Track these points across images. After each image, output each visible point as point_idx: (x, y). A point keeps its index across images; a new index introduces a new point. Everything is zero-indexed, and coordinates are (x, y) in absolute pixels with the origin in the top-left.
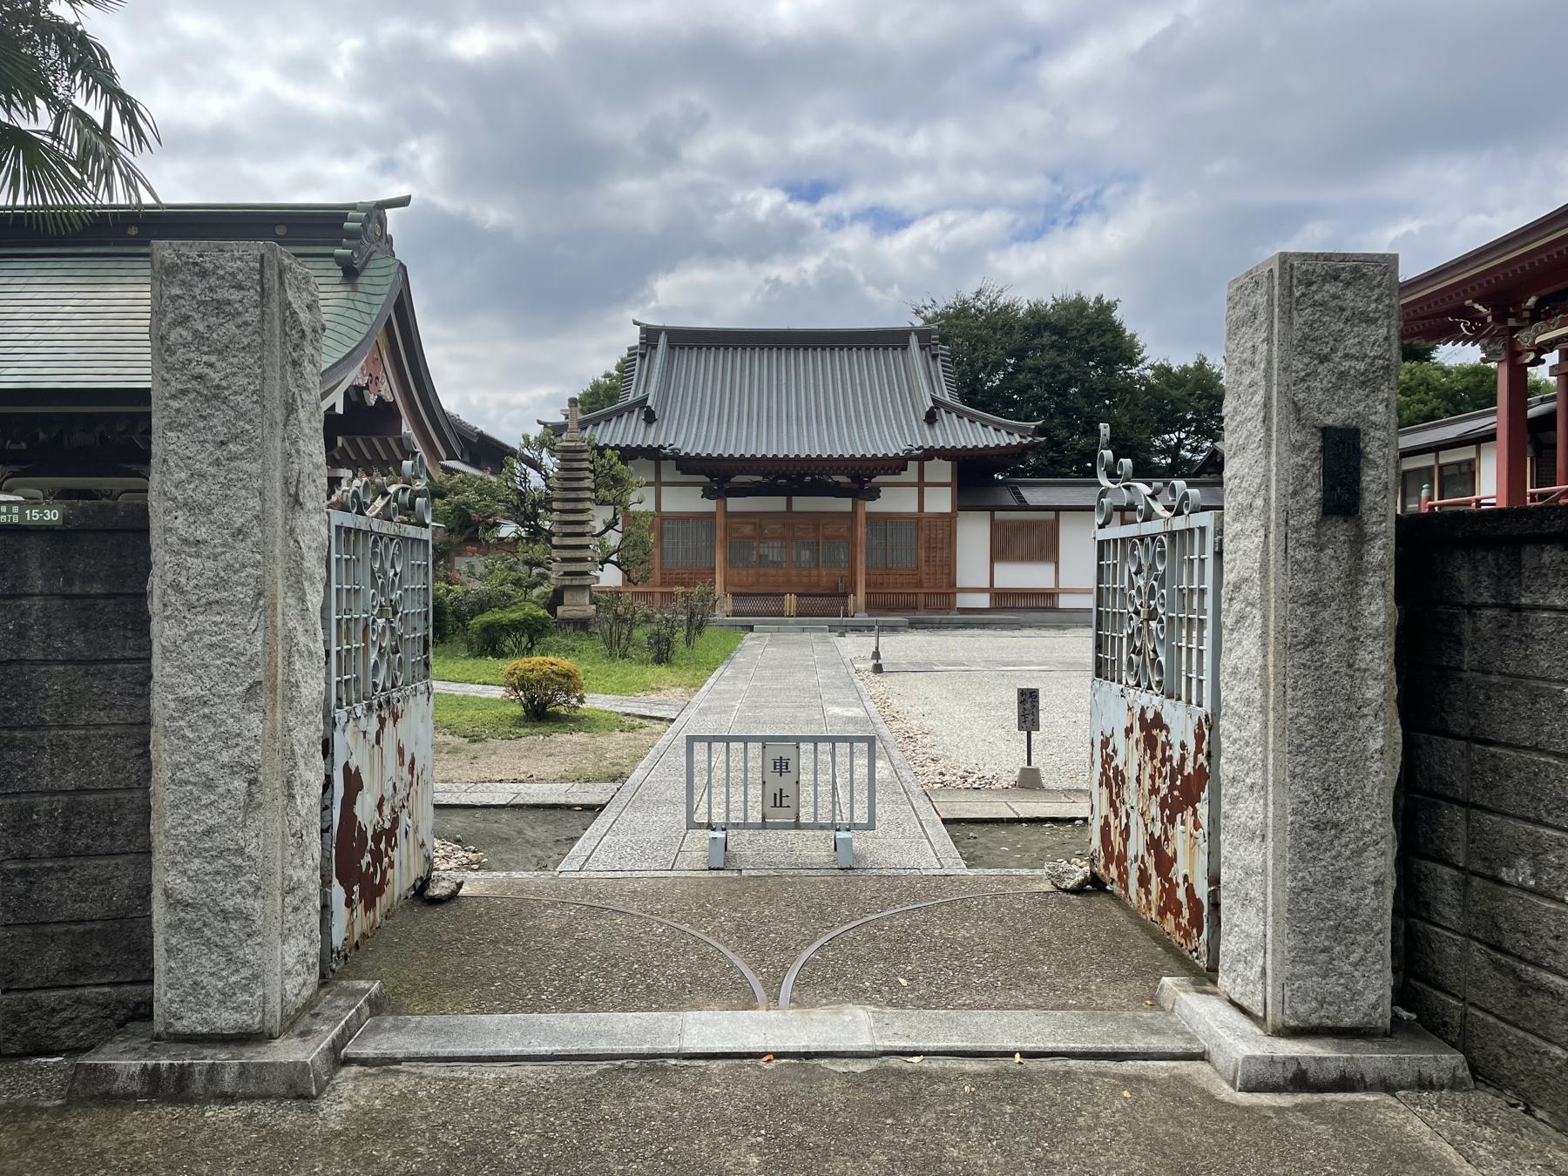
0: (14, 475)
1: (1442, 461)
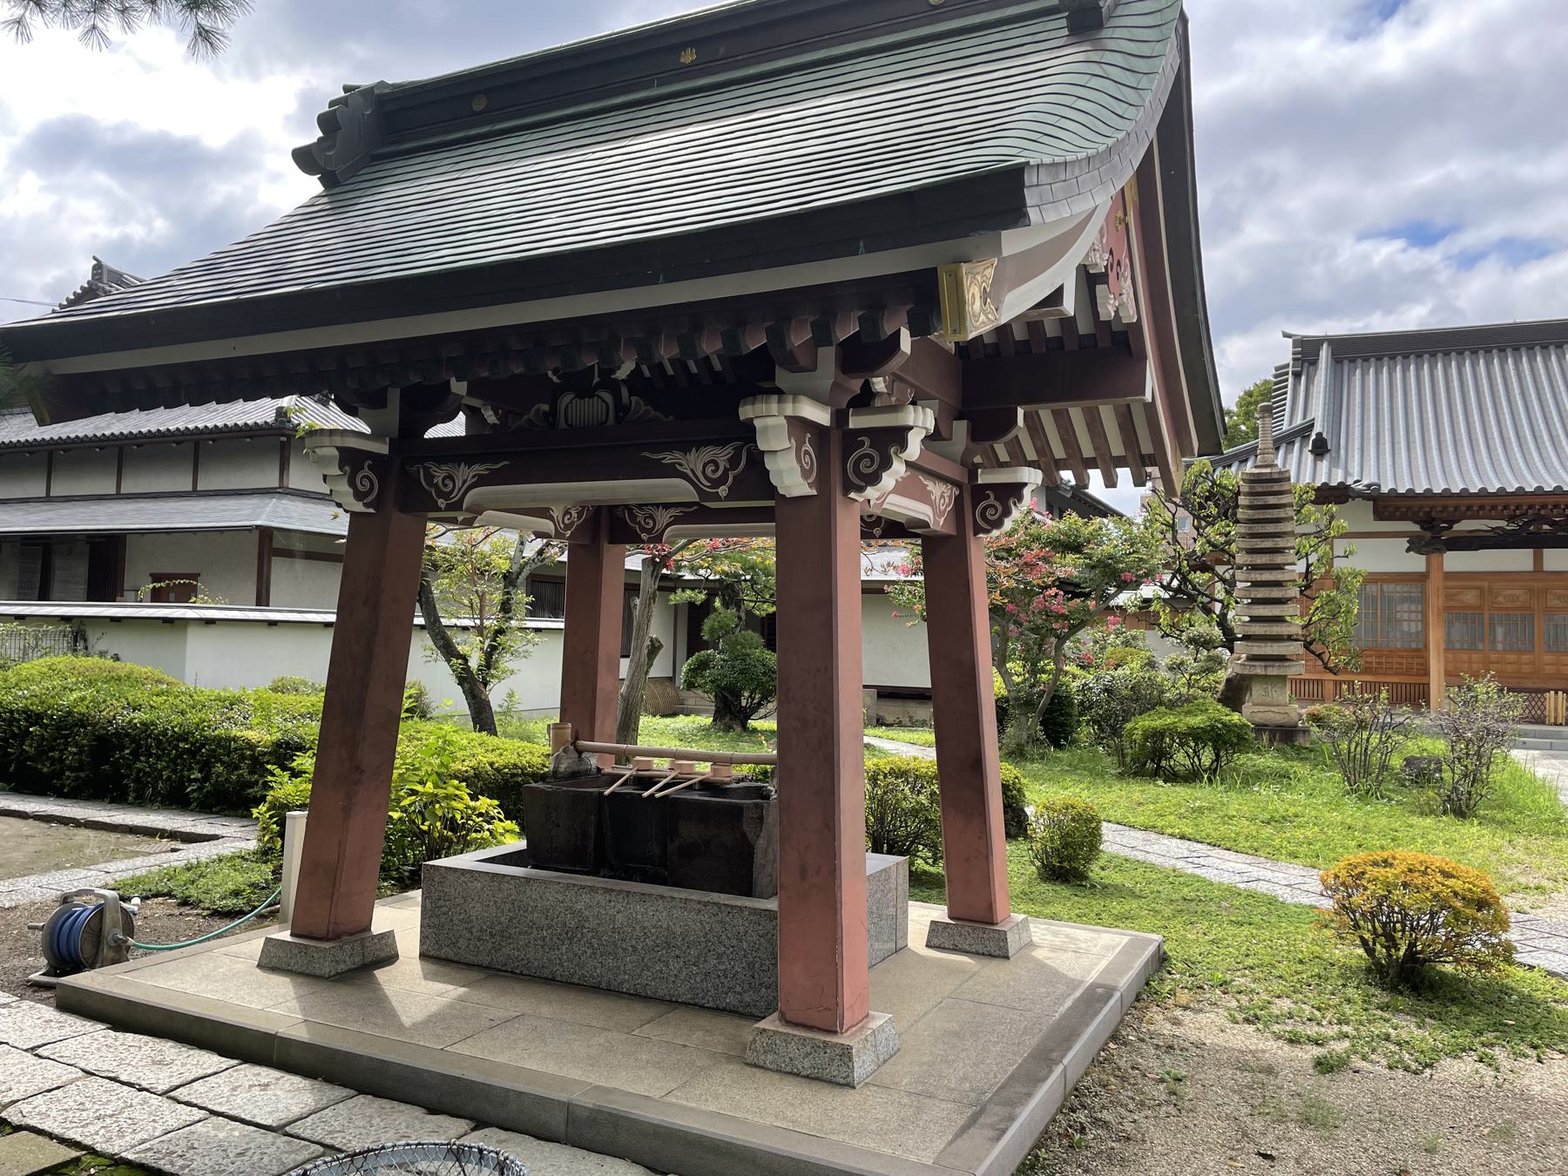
0: (481, 481)
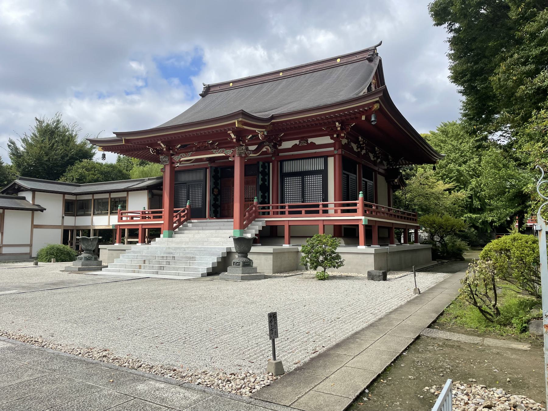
1: (95, 198)
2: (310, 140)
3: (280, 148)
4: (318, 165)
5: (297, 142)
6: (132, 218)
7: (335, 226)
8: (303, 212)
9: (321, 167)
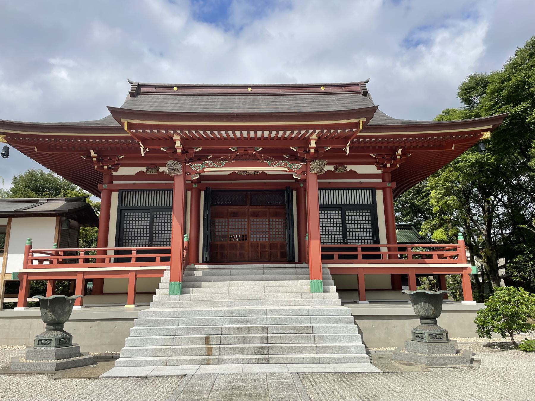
2: (349, 168)
3: (115, 174)
4: (363, 197)
5: (144, 169)
6: (41, 261)
7: (392, 276)
8: (336, 257)
9: (369, 201)
